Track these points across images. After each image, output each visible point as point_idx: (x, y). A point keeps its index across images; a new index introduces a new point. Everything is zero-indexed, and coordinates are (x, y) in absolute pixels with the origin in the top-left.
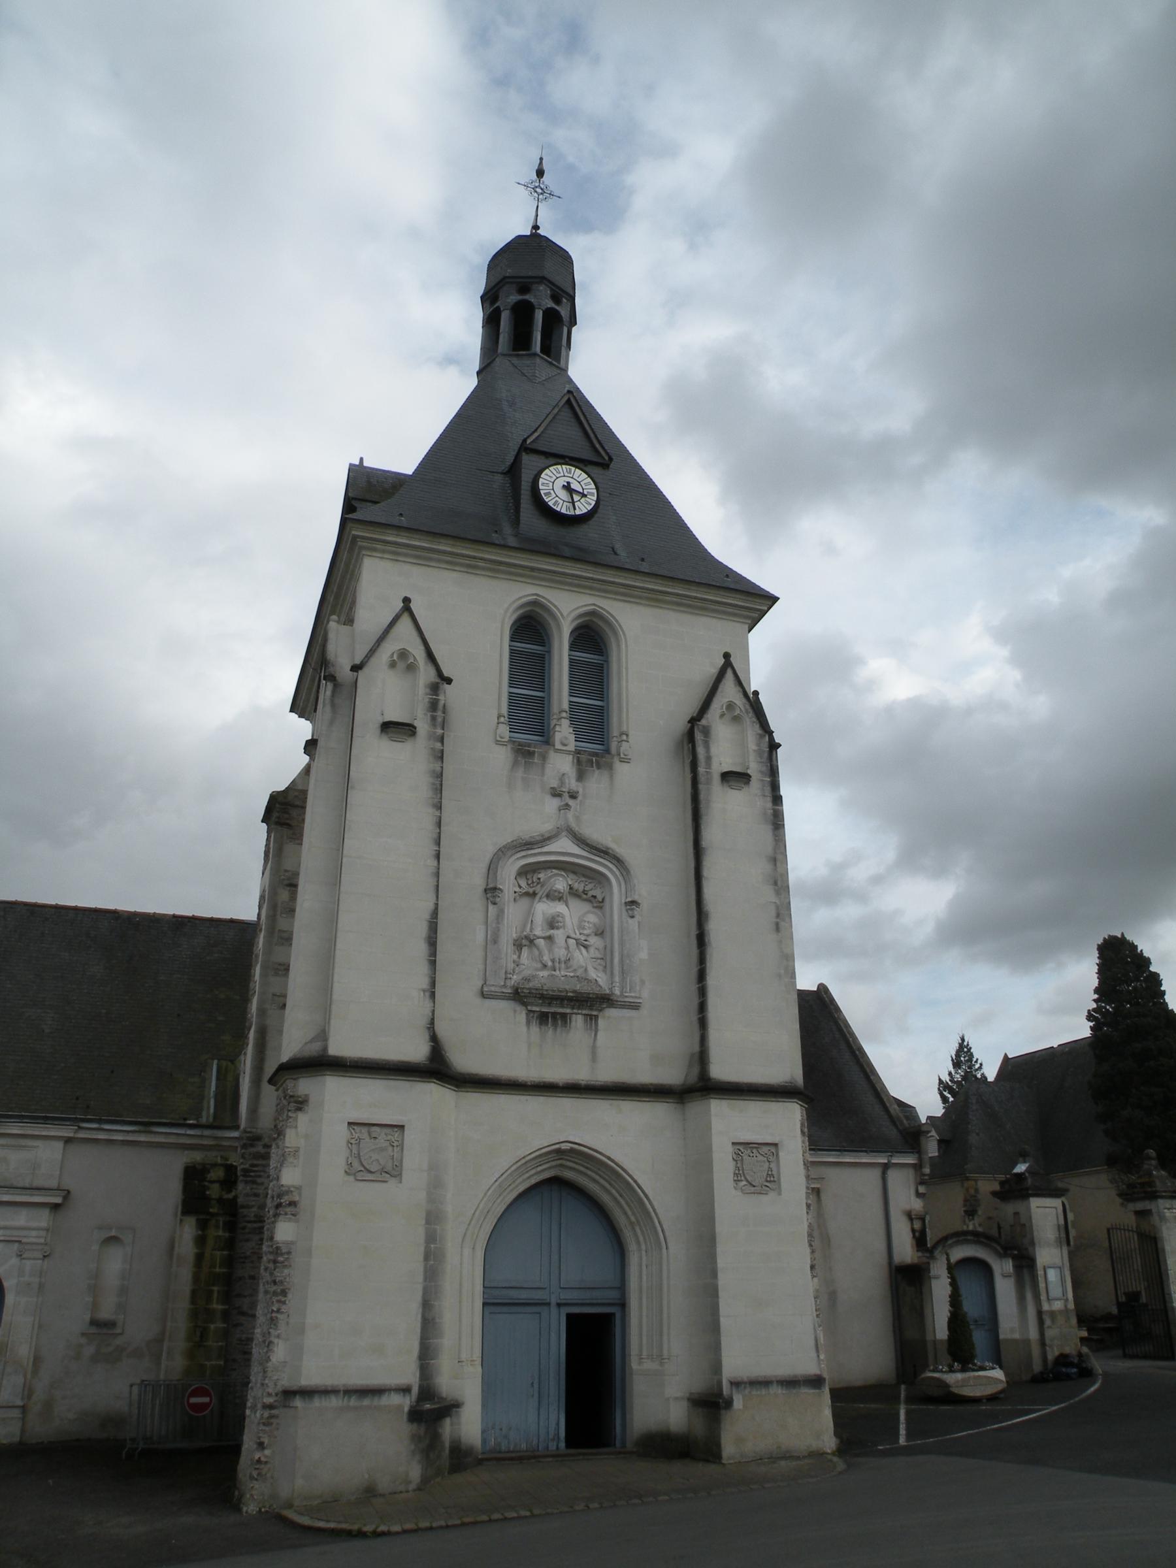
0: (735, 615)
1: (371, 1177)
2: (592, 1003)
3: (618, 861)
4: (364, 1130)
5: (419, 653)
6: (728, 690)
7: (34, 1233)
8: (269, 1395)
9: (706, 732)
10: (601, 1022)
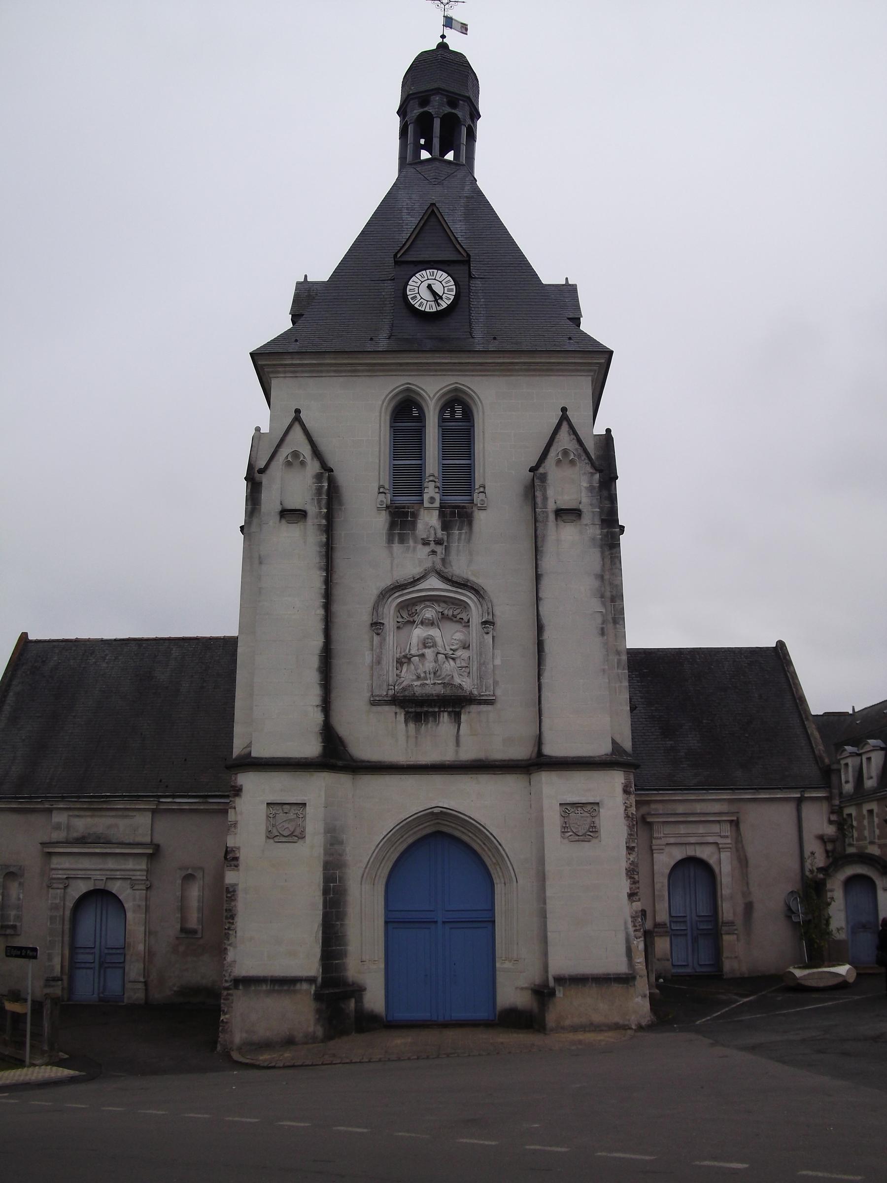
0: (577, 371)
1: (284, 839)
2: (455, 703)
3: (477, 591)
5: (306, 451)
6: (565, 440)
7: (138, 873)
8: (226, 981)
9: (543, 478)
10: (463, 717)
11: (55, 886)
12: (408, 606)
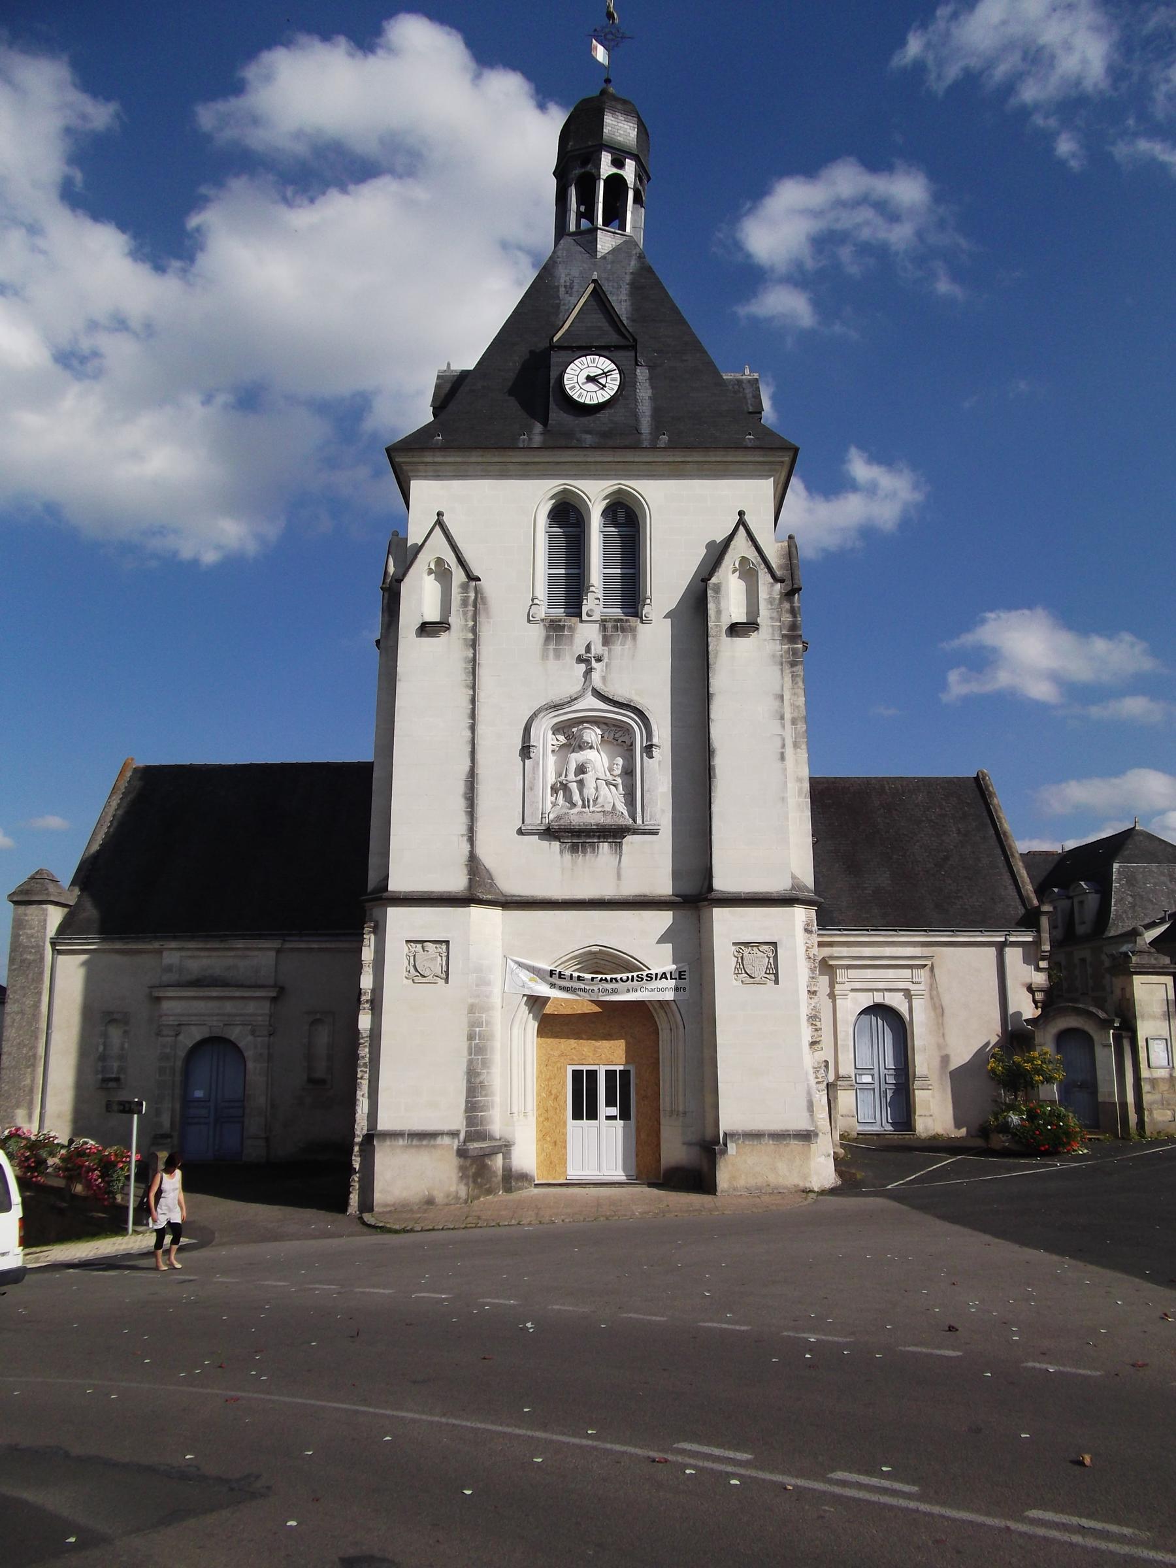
1: (424, 980)
4: (419, 946)
11: (165, 1033)
12: (563, 728)
